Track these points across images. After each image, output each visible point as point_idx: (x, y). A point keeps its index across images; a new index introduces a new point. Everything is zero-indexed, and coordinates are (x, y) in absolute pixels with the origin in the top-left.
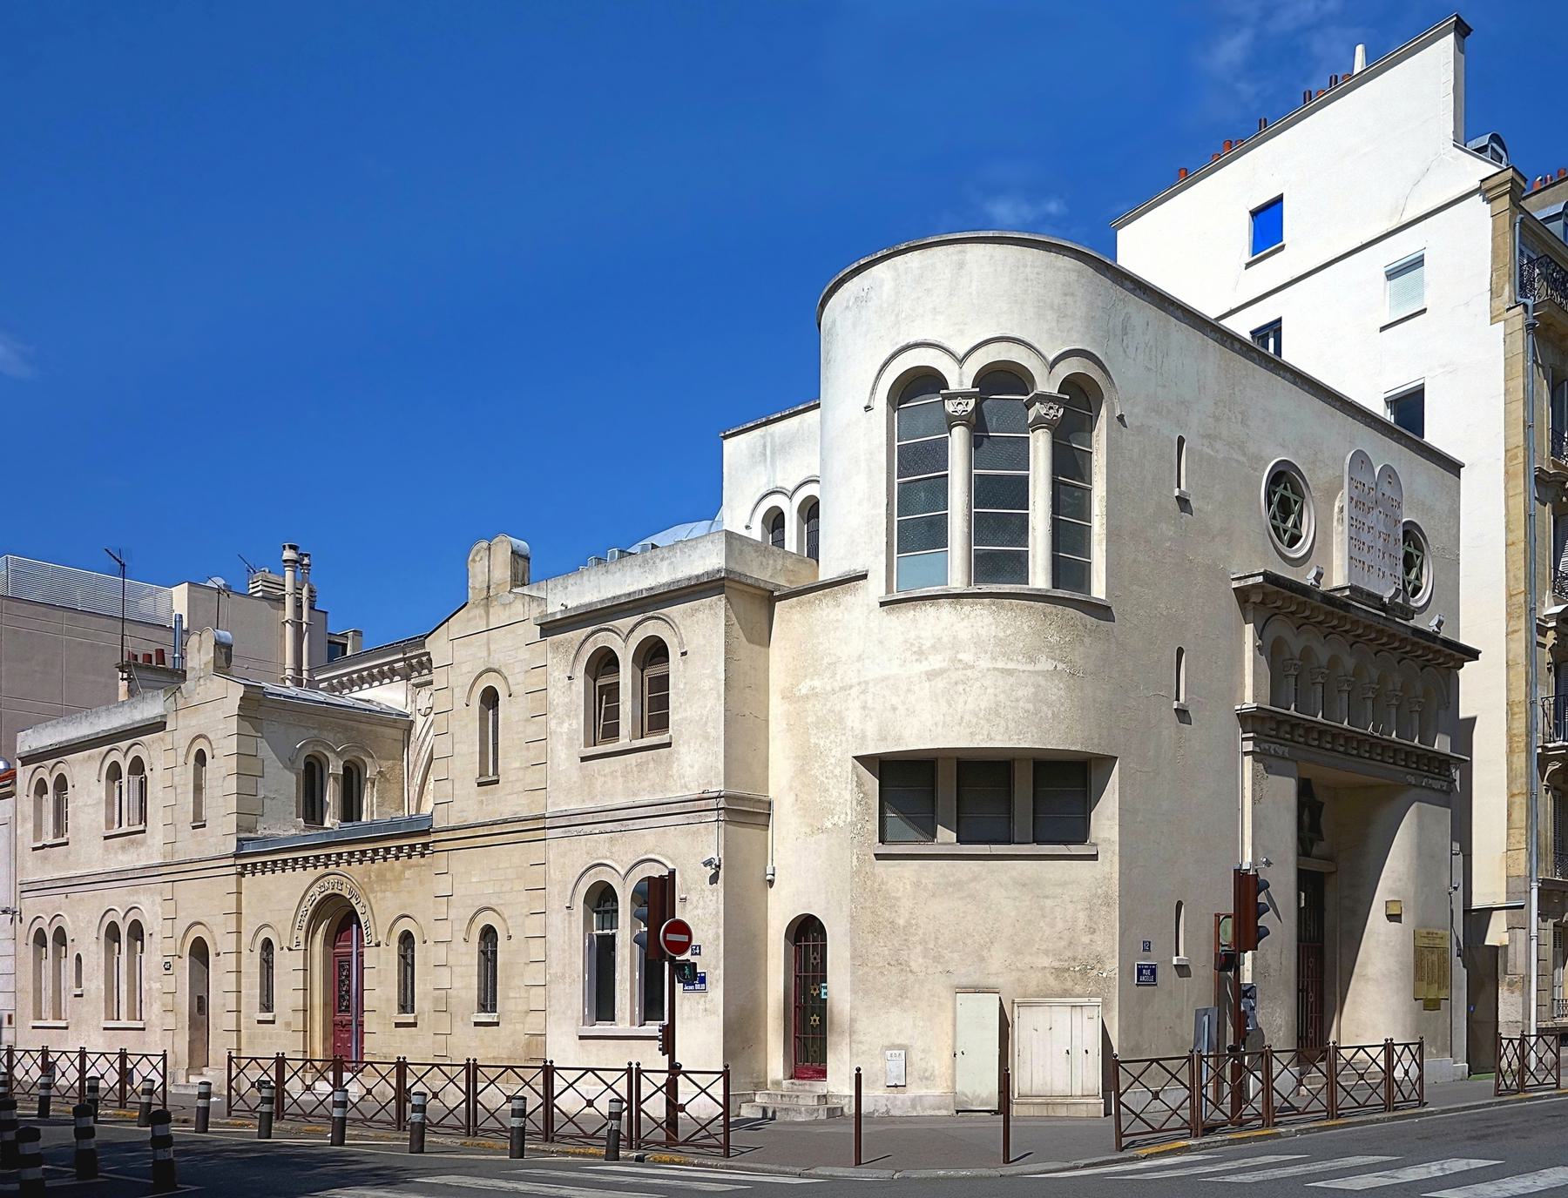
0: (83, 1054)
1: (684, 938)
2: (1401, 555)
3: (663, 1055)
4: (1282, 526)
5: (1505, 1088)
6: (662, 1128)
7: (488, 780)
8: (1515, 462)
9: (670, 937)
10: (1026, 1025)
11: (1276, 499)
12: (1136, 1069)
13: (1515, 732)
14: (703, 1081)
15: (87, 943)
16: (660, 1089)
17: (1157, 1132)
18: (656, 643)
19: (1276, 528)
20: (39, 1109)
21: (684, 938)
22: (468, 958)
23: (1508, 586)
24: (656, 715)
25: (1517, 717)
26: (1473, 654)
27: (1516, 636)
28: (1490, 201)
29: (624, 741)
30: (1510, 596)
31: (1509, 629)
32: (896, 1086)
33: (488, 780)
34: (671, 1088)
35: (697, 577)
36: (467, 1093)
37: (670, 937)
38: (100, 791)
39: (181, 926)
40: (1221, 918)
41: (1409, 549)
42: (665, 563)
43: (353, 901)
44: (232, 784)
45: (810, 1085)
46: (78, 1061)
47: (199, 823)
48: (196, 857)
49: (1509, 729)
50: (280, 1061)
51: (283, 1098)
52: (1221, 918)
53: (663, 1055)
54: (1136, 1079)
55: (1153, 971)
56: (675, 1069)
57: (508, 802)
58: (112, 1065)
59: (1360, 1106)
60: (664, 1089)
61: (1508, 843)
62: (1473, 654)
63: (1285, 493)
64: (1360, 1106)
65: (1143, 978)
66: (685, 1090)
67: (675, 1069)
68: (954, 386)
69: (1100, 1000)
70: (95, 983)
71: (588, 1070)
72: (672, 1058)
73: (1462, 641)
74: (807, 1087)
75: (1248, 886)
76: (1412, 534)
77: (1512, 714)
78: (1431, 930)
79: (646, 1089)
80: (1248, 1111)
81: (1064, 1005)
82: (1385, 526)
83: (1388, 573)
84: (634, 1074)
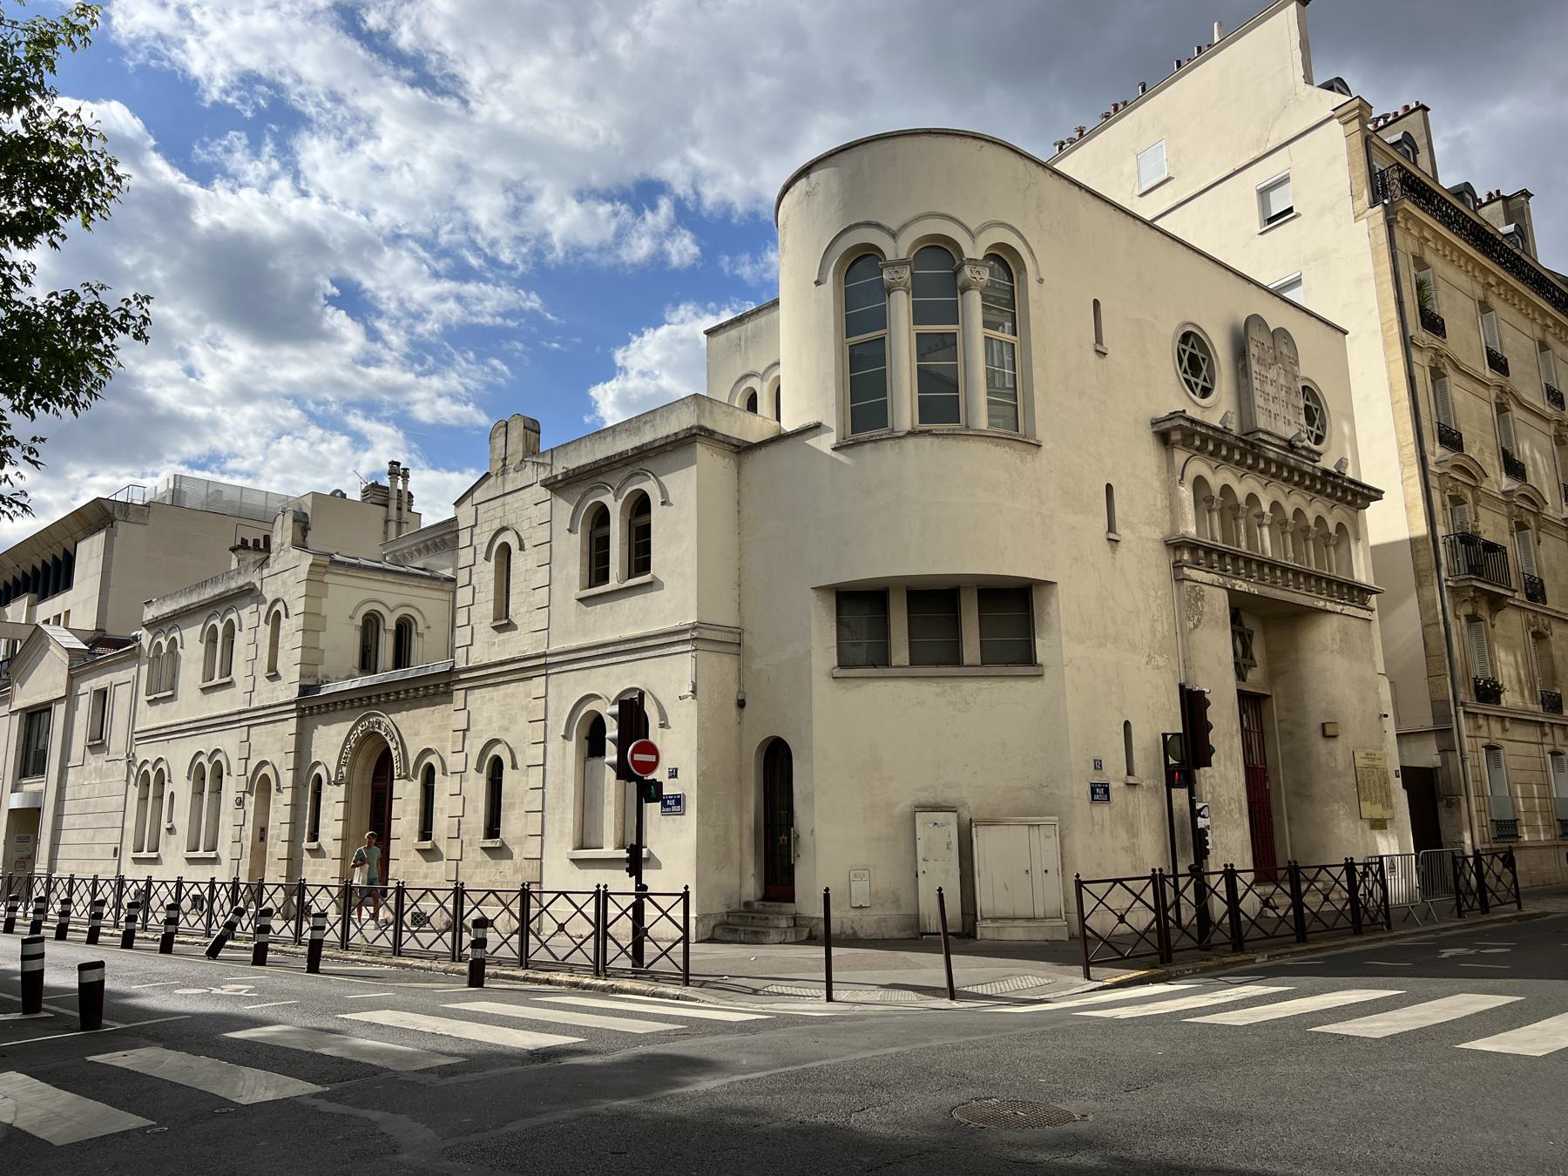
0: (95, 881)
1: (652, 758)
2: (1302, 406)
3: (631, 876)
4: (1193, 379)
5: (1369, 922)
6: (627, 953)
7: (504, 622)
8: (1391, 333)
9: (638, 757)
10: (984, 841)
11: (1185, 359)
12: (1099, 889)
13: (1421, 567)
14: (664, 902)
15: (180, 786)
16: (625, 912)
17: (560, 965)
18: (641, 496)
19: (1187, 381)
20: (172, 942)
21: (652, 758)
22: (478, 785)
23: (1398, 439)
24: (640, 560)
25: (1421, 553)
26: (1376, 494)
27: (1411, 481)
28: (1345, 123)
29: (613, 583)
30: (1401, 448)
31: (1405, 477)
32: (861, 907)
33: (504, 622)
34: (638, 909)
35: (676, 434)
36: (596, 925)
37: (638, 757)
38: (201, 649)
39: (252, 765)
40: (1169, 737)
41: (1308, 403)
42: (648, 426)
43: (388, 739)
44: (298, 639)
45: (779, 906)
46: (174, 890)
47: (274, 676)
48: (267, 704)
49: (1415, 566)
50: (212, 884)
51: (401, 931)
52: (1169, 737)
53: (631, 876)
54: (1101, 901)
55: (1107, 791)
56: (642, 892)
57: (518, 644)
58: (442, 905)
59: (1268, 936)
60: (630, 912)
61: (1428, 670)
62: (1376, 494)
63: (1193, 351)
64: (1268, 936)
65: (1096, 797)
66: (650, 912)
67: (642, 892)
68: (890, 256)
69: (1056, 818)
70: (182, 820)
71: (560, 893)
72: (639, 880)
73: (1364, 481)
74: (777, 909)
75: (1193, 703)
76: (1309, 392)
77: (1417, 551)
78: (1369, 751)
79: (613, 911)
80: (1217, 937)
81: (1020, 824)
82: (1286, 380)
83: (1292, 420)
84: (602, 897)
